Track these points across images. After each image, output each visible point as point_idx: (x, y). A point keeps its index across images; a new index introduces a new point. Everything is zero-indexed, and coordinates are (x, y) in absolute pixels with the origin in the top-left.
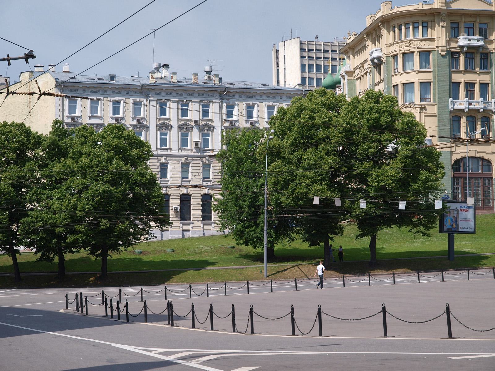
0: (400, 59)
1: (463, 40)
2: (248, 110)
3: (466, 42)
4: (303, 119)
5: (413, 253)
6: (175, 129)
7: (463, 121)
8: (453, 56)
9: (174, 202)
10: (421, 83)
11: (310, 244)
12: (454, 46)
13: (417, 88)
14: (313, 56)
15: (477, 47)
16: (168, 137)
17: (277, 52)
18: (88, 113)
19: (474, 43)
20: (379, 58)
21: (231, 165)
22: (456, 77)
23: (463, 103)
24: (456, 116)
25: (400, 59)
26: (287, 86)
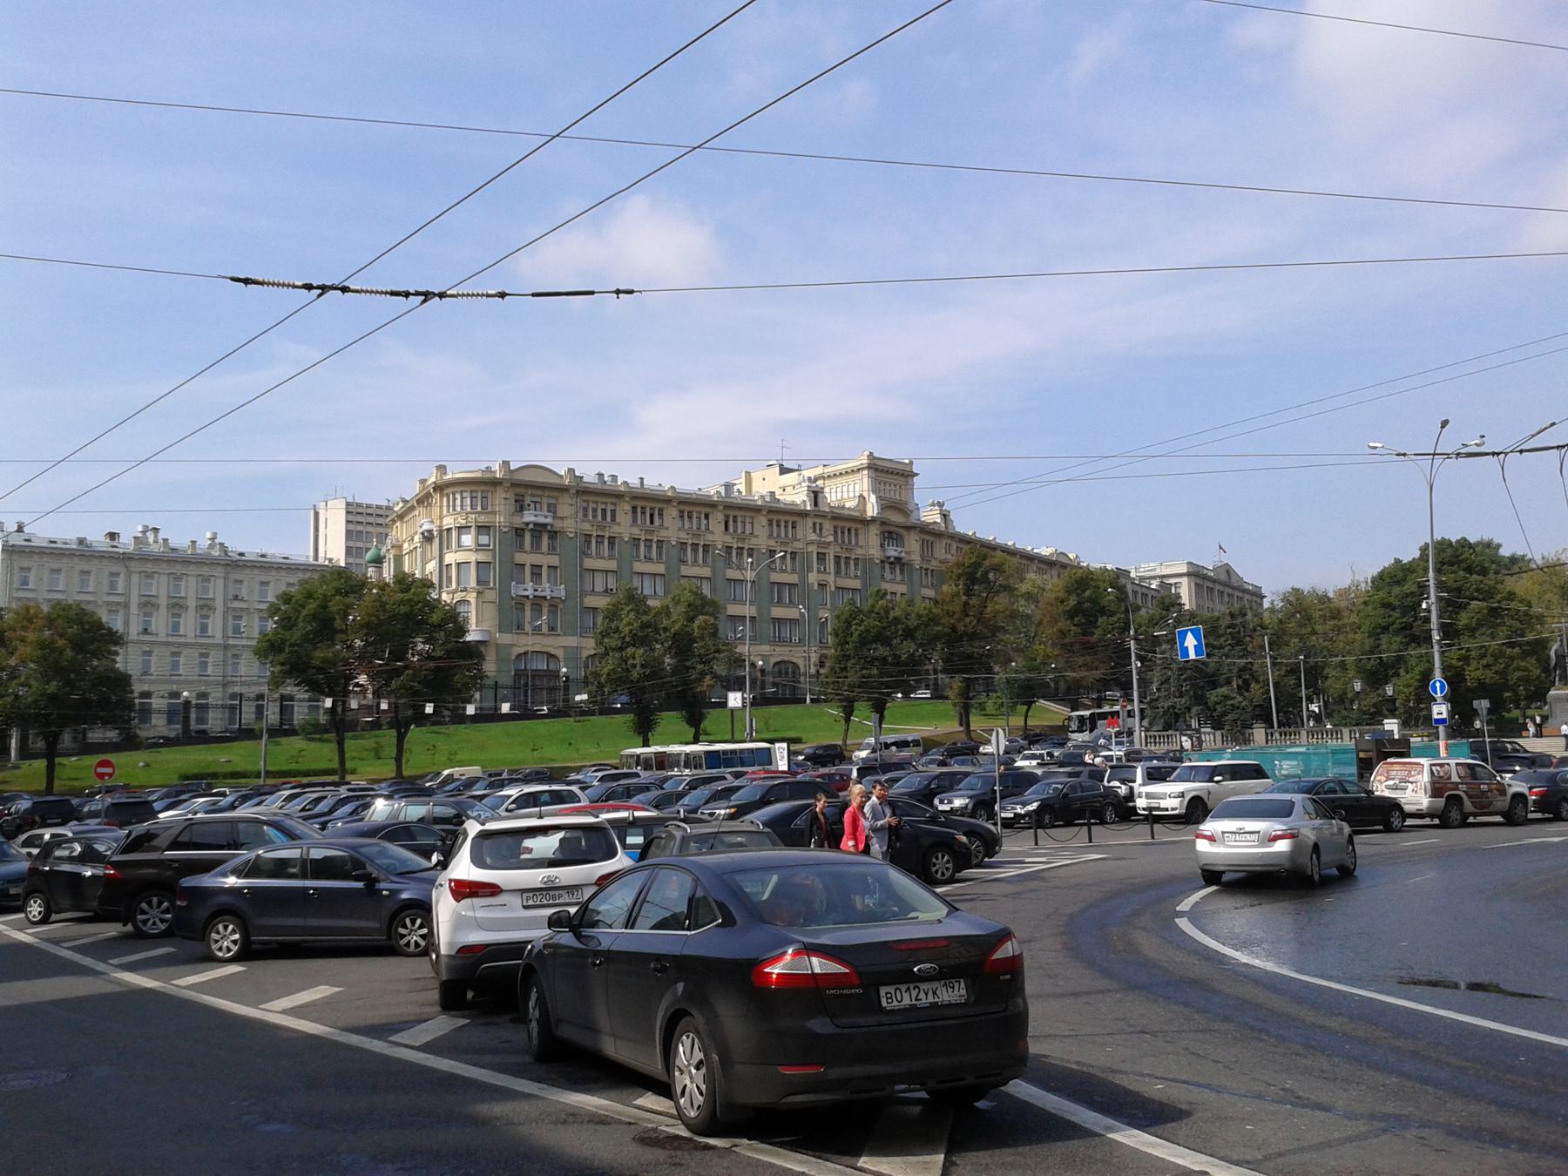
0: (454, 534)
1: (529, 517)
2: (351, 544)
3: (532, 519)
4: (312, 606)
5: (1300, 1001)
6: (191, 612)
7: (528, 608)
8: (519, 532)
9: (679, 1091)
10: (478, 563)
12: (518, 521)
13: (473, 567)
14: (365, 522)
15: (544, 525)
16: (182, 621)
17: (316, 515)
18: (106, 589)
19: (541, 520)
20: (430, 531)
21: (1392, 600)
22: (520, 558)
23: (528, 589)
24: (520, 602)
25: (454, 534)
26: (321, 561)
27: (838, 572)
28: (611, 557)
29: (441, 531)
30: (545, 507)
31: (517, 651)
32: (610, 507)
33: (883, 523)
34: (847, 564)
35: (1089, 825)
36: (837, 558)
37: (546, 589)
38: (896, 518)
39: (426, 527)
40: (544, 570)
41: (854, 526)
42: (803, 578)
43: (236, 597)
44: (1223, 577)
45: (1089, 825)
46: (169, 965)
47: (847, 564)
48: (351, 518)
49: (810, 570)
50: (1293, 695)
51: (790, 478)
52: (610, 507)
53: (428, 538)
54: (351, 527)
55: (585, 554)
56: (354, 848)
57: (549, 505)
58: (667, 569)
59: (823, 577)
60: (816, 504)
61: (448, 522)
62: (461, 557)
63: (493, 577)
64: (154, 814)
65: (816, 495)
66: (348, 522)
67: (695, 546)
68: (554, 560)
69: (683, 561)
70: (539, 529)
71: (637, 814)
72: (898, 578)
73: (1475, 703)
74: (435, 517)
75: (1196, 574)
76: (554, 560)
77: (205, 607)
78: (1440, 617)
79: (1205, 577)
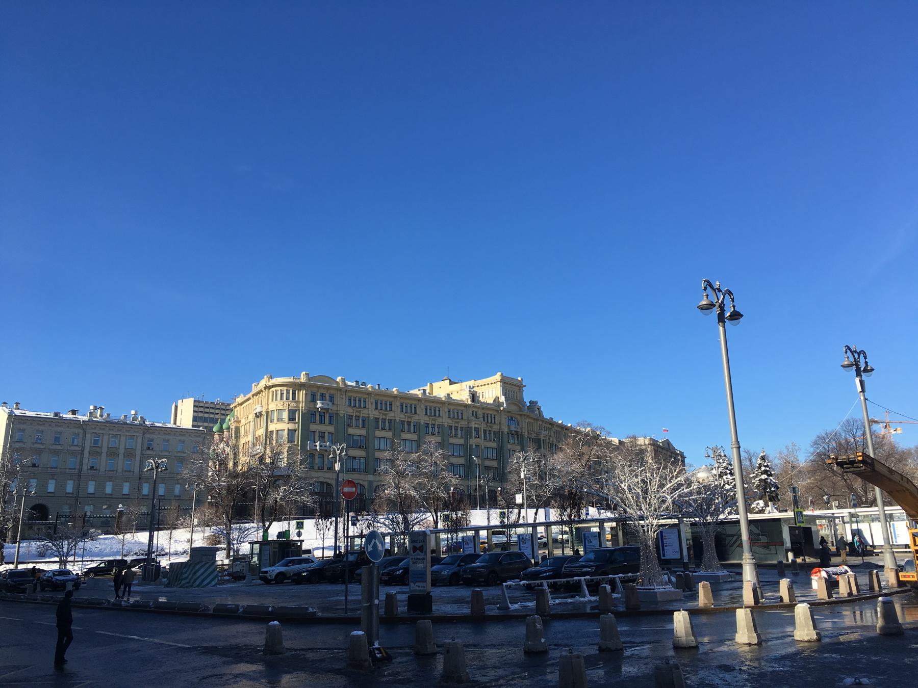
22: (313, 427)
27: (485, 439)
29: (267, 413)
31: (375, 484)
33: (509, 412)
36: (485, 431)
39: (258, 410)
40: (326, 435)
43: (148, 448)
48: (196, 409)
49: (471, 437)
53: (258, 415)
54: (196, 414)
59: (479, 440)
61: (272, 406)
64: (545, 674)
65: (474, 396)
68: (331, 429)
71: (21, 567)
72: (516, 442)
74: (264, 404)
76: (331, 429)
79: (659, 446)
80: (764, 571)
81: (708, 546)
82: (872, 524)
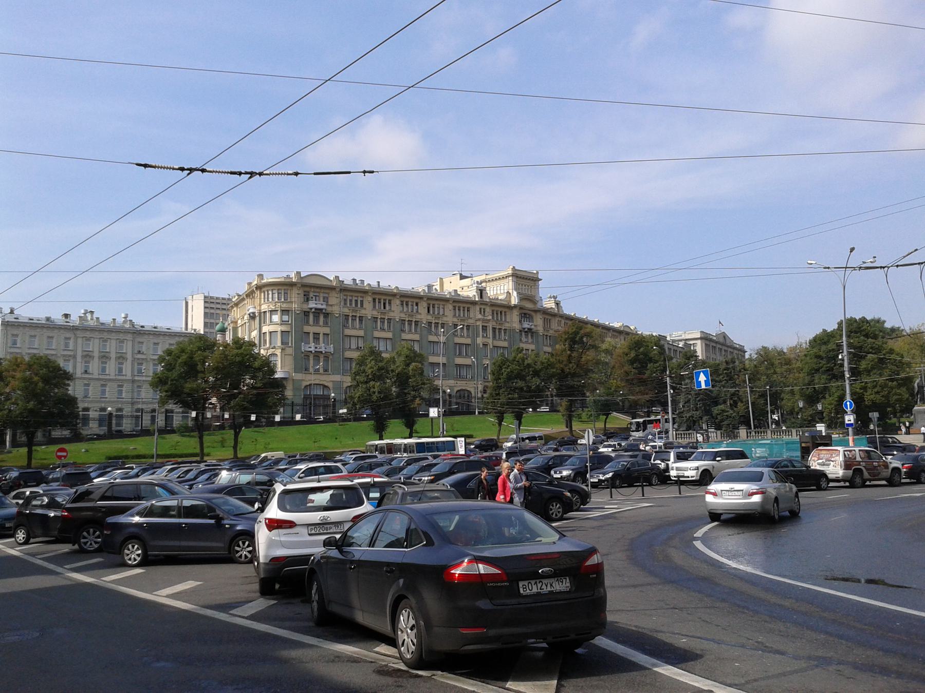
0: (268, 315)
1: (312, 305)
2: (207, 321)
3: (314, 306)
4: (184, 357)
5: (767, 590)
6: (113, 361)
7: (311, 358)
8: (306, 314)
10: (282, 332)
11: (68, 379)
12: (306, 307)
13: (279, 334)
14: (216, 308)
15: (321, 309)
16: (107, 366)
17: (187, 303)
18: (62, 347)
19: (319, 306)
20: (254, 313)
22: (307, 329)
23: (312, 347)
24: (307, 355)
25: (268, 315)
26: (189, 331)
27: (494, 337)
28: (360, 328)
29: (260, 313)
30: (322, 299)
31: (305, 384)
32: (360, 299)
33: (521, 308)
34: (500, 332)
35: (643, 486)
36: (494, 329)
37: (322, 347)
38: (529, 305)
39: (251, 311)
40: (321, 336)
41: (504, 310)
42: (474, 341)
43: (139, 352)
44: (721, 340)
45: (643, 486)
46: (100, 569)
47: (500, 332)
48: (207, 305)
49: (478, 336)
50: (763, 410)
51: (466, 282)
52: (360, 299)
53: (252, 317)
54: (207, 310)
55: (345, 326)
56: (209, 500)
57: (324, 298)
58: (394, 335)
59: (485, 340)
60: (481, 297)
61: (264, 307)
62: (272, 328)
63: (291, 340)
65: (481, 292)
66: (205, 308)
67: (410, 322)
68: (327, 330)
69: (403, 331)
70: (318, 312)
72: (530, 340)
73: (870, 414)
74: (257, 305)
75: (706, 338)
76: (327, 330)
77: (121, 358)
78: (849, 363)
79: (711, 340)
80: (524, 282)
81: (817, 666)
82: (682, 487)
